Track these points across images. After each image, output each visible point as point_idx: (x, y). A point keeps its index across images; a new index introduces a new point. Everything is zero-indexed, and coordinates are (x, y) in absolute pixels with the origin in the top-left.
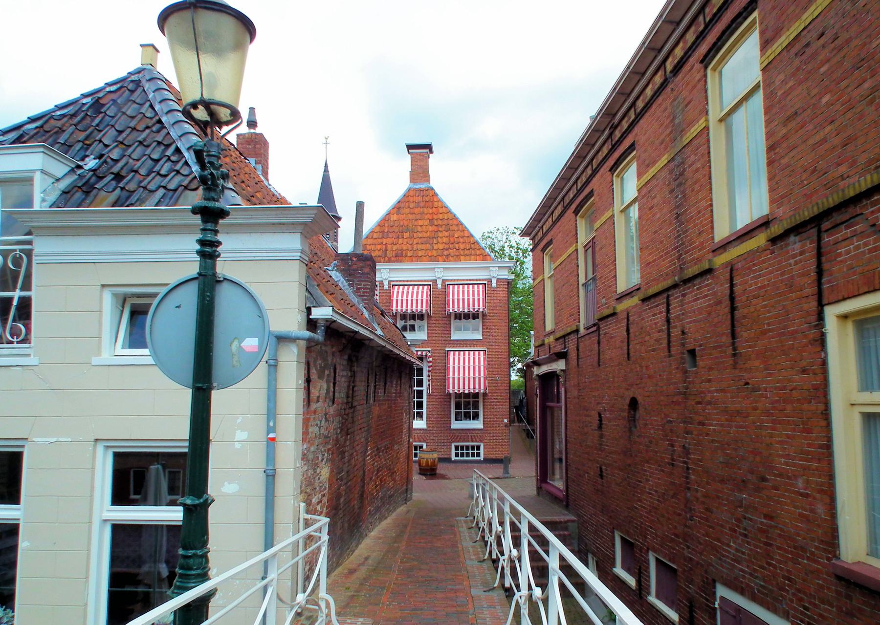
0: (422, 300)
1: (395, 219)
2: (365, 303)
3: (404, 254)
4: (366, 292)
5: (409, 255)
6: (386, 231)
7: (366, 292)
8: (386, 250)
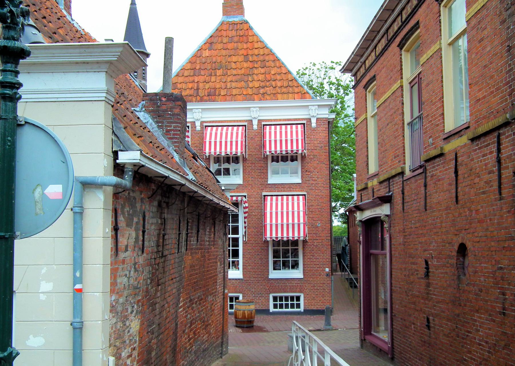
1: (207, 55)
3: (217, 93)
6: (197, 68)
8: (198, 89)
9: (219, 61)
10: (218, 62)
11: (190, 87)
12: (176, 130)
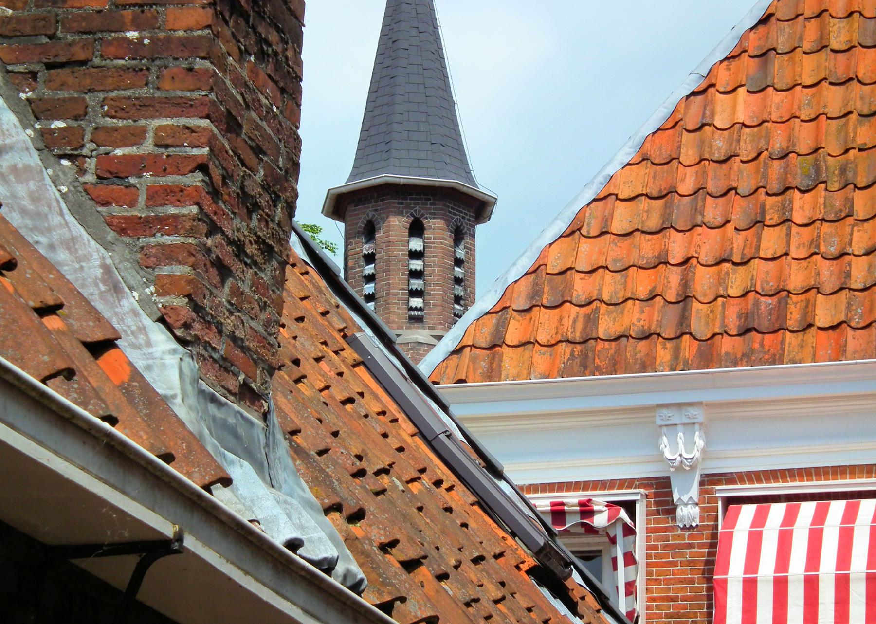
0: (842, 584)
1: (741, 118)
2: (164, 287)
3: (794, 318)
4: (177, 194)
5: (822, 319)
6: (686, 187)
7: (177, 194)
8: (685, 299)
9: (804, 145)
10: (803, 151)
11: (642, 292)
12: (177, 166)
